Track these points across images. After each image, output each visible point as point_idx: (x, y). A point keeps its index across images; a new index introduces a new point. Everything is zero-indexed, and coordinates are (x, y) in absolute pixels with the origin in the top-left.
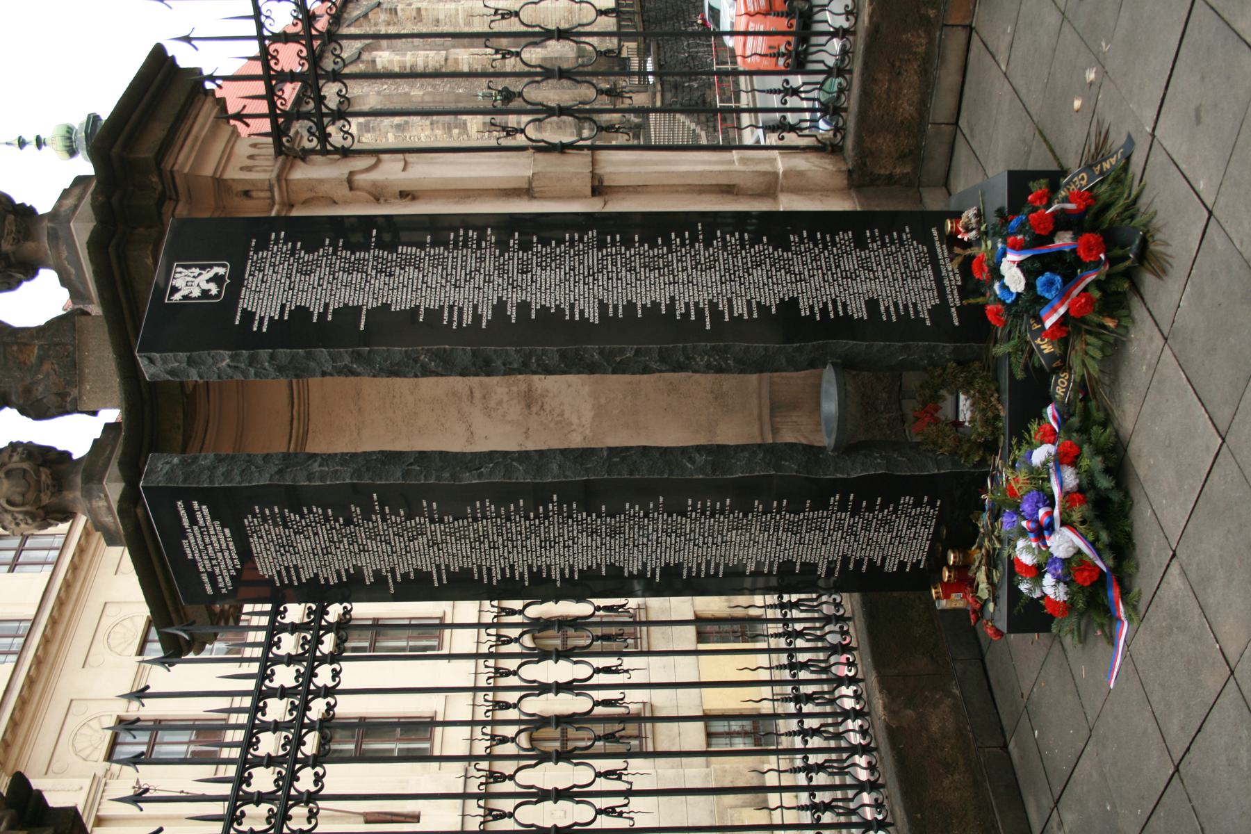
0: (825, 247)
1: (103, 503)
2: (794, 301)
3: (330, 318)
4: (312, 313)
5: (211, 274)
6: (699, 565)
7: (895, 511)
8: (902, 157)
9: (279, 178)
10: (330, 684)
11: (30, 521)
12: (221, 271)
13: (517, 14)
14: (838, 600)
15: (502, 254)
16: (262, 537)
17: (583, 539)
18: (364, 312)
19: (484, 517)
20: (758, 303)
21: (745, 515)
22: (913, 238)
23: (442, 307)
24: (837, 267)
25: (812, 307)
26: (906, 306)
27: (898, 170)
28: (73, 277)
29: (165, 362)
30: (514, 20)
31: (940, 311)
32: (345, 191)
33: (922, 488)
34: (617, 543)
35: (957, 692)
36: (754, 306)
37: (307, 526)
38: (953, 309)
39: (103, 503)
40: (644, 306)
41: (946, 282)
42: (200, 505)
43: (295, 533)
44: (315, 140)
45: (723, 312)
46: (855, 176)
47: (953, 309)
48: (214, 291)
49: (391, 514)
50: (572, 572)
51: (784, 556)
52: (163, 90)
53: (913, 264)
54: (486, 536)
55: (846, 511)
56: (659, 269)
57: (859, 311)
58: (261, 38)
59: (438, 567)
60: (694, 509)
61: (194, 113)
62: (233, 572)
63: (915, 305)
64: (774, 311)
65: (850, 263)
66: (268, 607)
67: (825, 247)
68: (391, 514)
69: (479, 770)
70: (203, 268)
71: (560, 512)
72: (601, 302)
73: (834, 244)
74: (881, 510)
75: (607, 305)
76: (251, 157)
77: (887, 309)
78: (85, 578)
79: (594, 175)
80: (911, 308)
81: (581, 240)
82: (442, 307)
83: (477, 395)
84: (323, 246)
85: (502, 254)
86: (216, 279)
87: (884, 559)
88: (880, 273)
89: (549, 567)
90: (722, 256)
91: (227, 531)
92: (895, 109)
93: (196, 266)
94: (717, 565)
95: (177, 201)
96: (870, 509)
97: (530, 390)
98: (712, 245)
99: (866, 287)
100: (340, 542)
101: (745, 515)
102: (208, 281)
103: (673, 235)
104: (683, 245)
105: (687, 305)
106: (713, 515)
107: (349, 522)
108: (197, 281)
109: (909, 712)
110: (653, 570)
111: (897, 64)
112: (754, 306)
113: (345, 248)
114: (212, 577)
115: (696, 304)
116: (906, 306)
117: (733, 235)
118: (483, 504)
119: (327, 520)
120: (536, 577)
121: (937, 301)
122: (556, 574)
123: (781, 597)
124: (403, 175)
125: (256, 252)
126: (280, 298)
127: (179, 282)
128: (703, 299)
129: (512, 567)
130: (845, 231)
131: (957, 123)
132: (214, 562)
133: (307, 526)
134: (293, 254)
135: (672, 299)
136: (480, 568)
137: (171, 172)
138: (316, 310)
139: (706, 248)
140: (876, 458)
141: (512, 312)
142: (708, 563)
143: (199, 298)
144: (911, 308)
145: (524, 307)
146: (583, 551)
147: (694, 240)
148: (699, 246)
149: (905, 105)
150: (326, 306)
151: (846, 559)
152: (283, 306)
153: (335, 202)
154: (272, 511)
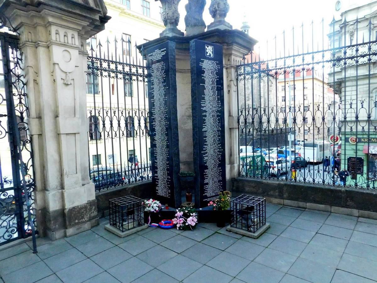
0: (219, 174)
2: (208, 169)
7: (167, 189)
12: (212, 56)
25: (206, 172)
26: (207, 190)
40: (206, 139)
67: (219, 174)
70: (212, 52)
71: (166, 124)
76: (236, 61)
77: (206, 187)
81: (219, 127)
86: (210, 55)
89: (155, 122)
94: (156, 154)
99: (211, 182)
105: (206, 148)
110: (155, 142)
113: (217, 80)
115: (207, 150)
116: (207, 190)
119: (163, 78)
122: (154, 123)
124: (233, 91)
135: (208, 145)
138: (204, 75)
145: (205, 116)
152: (205, 68)
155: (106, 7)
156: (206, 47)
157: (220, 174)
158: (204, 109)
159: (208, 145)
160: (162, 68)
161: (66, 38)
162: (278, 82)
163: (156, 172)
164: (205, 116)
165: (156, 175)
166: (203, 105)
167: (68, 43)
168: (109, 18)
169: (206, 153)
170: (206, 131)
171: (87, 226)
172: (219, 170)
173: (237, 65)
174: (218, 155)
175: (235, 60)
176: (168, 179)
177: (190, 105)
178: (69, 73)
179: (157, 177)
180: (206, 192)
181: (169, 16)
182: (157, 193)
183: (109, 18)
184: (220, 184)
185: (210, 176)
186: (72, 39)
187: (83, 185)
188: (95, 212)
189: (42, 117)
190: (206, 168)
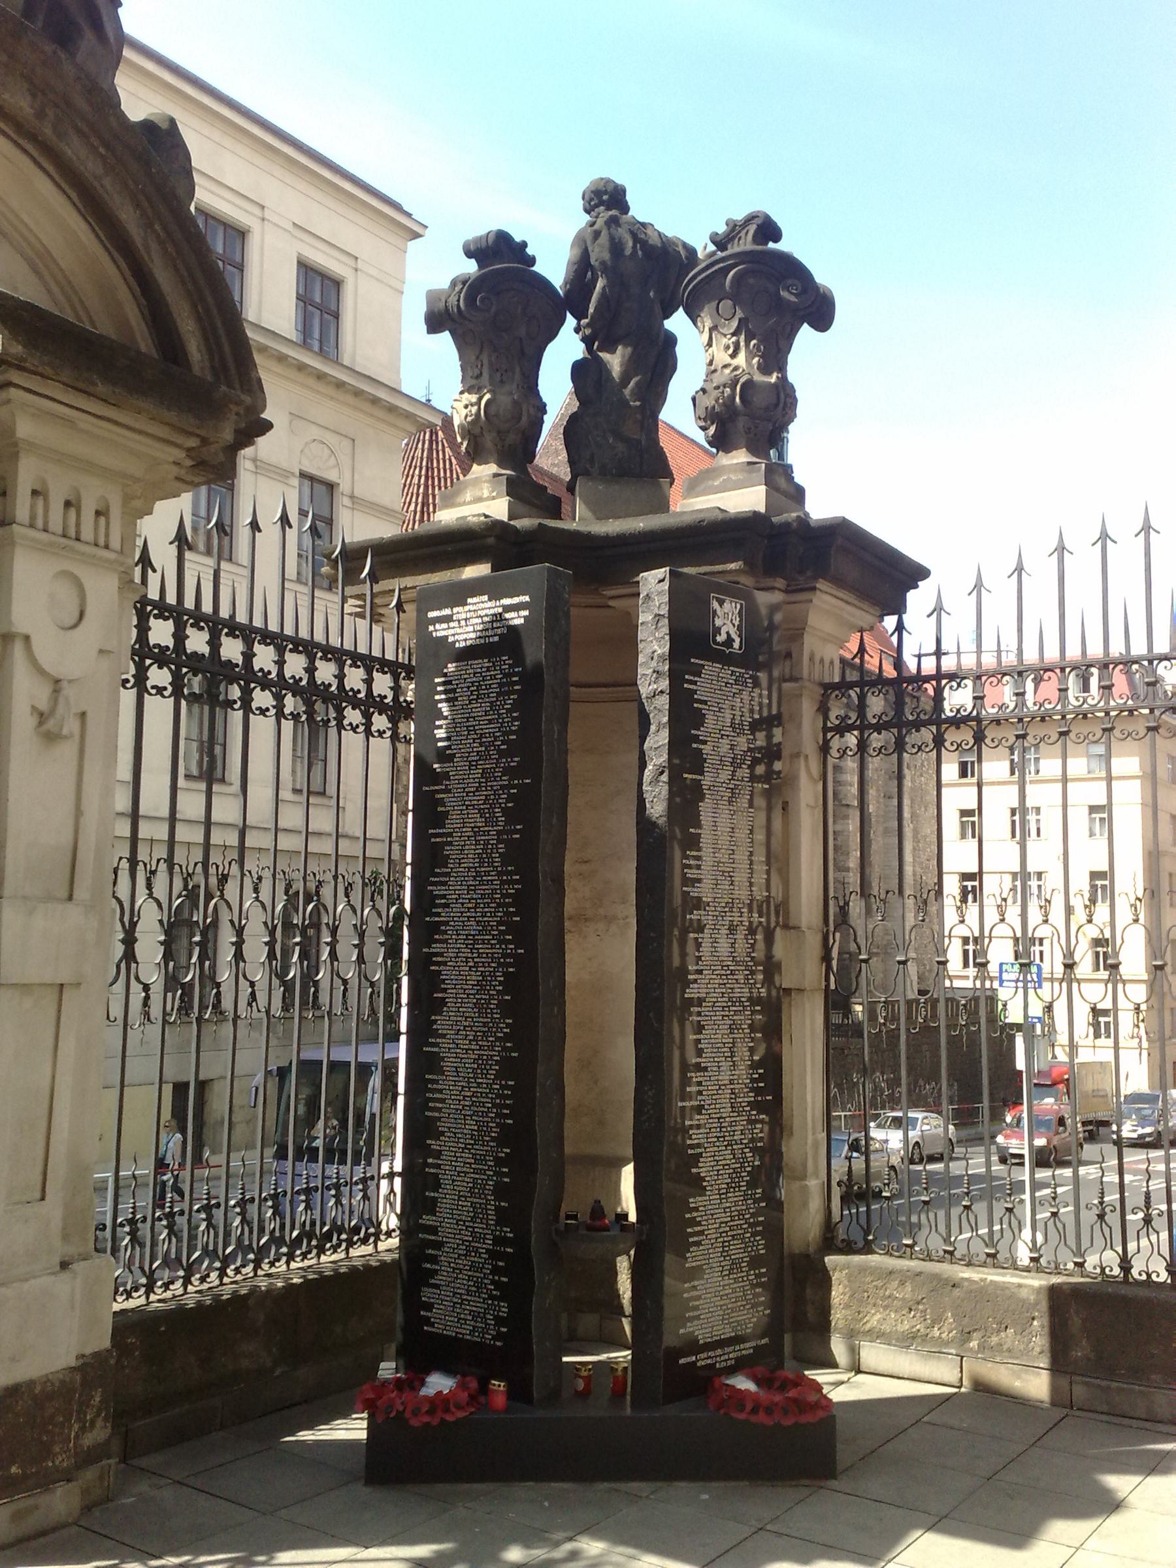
0: (751, 1225)
1: (486, 494)
3: (694, 746)
4: (699, 730)
5: (734, 636)
6: (440, 1091)
7: (491, 1297)
11: (469, 419)
12: (736, 645)
14: (393, 1234)
16: (488, 670)
17: (475, 977)
19: (503, 882)
21: (493, 1139)
24: (733, 1236)
25: (696, 1209)
26: (696, 1308)
28: (710, 483)
29: (659, 593)
33: (518, 1323)
34: (468, 1009)
36: (699, 1150)
37: (499, 714)
38: (694, 1358)
39: (486, 494)
41: (719, 1352)
42: (525, 617)
43: (491, 703)
44: (837, 722)
47: (694, 1358)
48: (719, 639)
49: (509, 794)
50: (438, 964)
51: (445, 1180)
52: (885, 577)
54: (482, 883)
55: (493, 1245)
56: (732, 1057)
58: (939, 676)
59: (450, 835)
60: (503, 1087)
61: (865, 607)
62: (451, 639)
63: (698, 1317)
64: (694, 1170)
68: (509, 794)
69: (230, 864)
70: (739, 628)
71: (505, 956)
73: (754, 1234)
74: (493, 1282)
76: (822, 661)
78: (65, 192)
80: (696, 1313)
82: (699, 850)
83: (584, 867)
86: (729, 641)
87: (437, 1286)
88: (726, 1282)
89: (445, 941)
91: (496, 639)
93: (741, 621)
94: (439, 1110)
95: (786, 591)
96: (495, 1270)
97: (586, 920)
98: (752, 1110)
100: (481, 745)
101: (493, 1139)
102: (728, 633)
103: (761, 1071)
106: (494, 1105)
107: (502, 754)
108: (729, 622)
109: (262, 1317)
110: (436, 1045)
111: (921, 1307)
112: (699, 1150)
114: (448, 619)
118: (516, 882)
119: (505, 734)
120: (435, 928)
121: (701, 1342)
122: (436, 948)
123: (399, 1174)
124: (803, 805)
127: (727, 605)
129: (446, 906)
130: (766, 1247)
132: (463, 623)
133: (499, 714)
135: (705, 1069)
136: (448, 875)
137: (814, 589)
138: (700, 733)
142: (443, 1101)
143: (714, 625)
144: (696, 1313)
146: (460, 976)
149: (878, 1316)
151: (439, 1245)
152: (705, 702)
154: (516, 683)
155: (259, 380)
156: (715, 605)
157: (758, 1224)
159: (705, 1069)
160: (500, 685)
161: (40, 503)
162: (1031, 782)
163: (431, 1207)
165: (427, 1220)
167: (78, 539)
168: (267, 426)
170: (700, 1002)
171: (61, 1501)
173: (827, 681)
175: (817, 659)
176: (497, 1241)
178: (70, 681)
179: (433, 1230)
181: (497, 415)
182: (427, 1320)
183: (267, 426)
184: (757, 1276)
185: (712, 1233)
186: (96, 522)
187: (64, 1265)
188: (99, 1423)
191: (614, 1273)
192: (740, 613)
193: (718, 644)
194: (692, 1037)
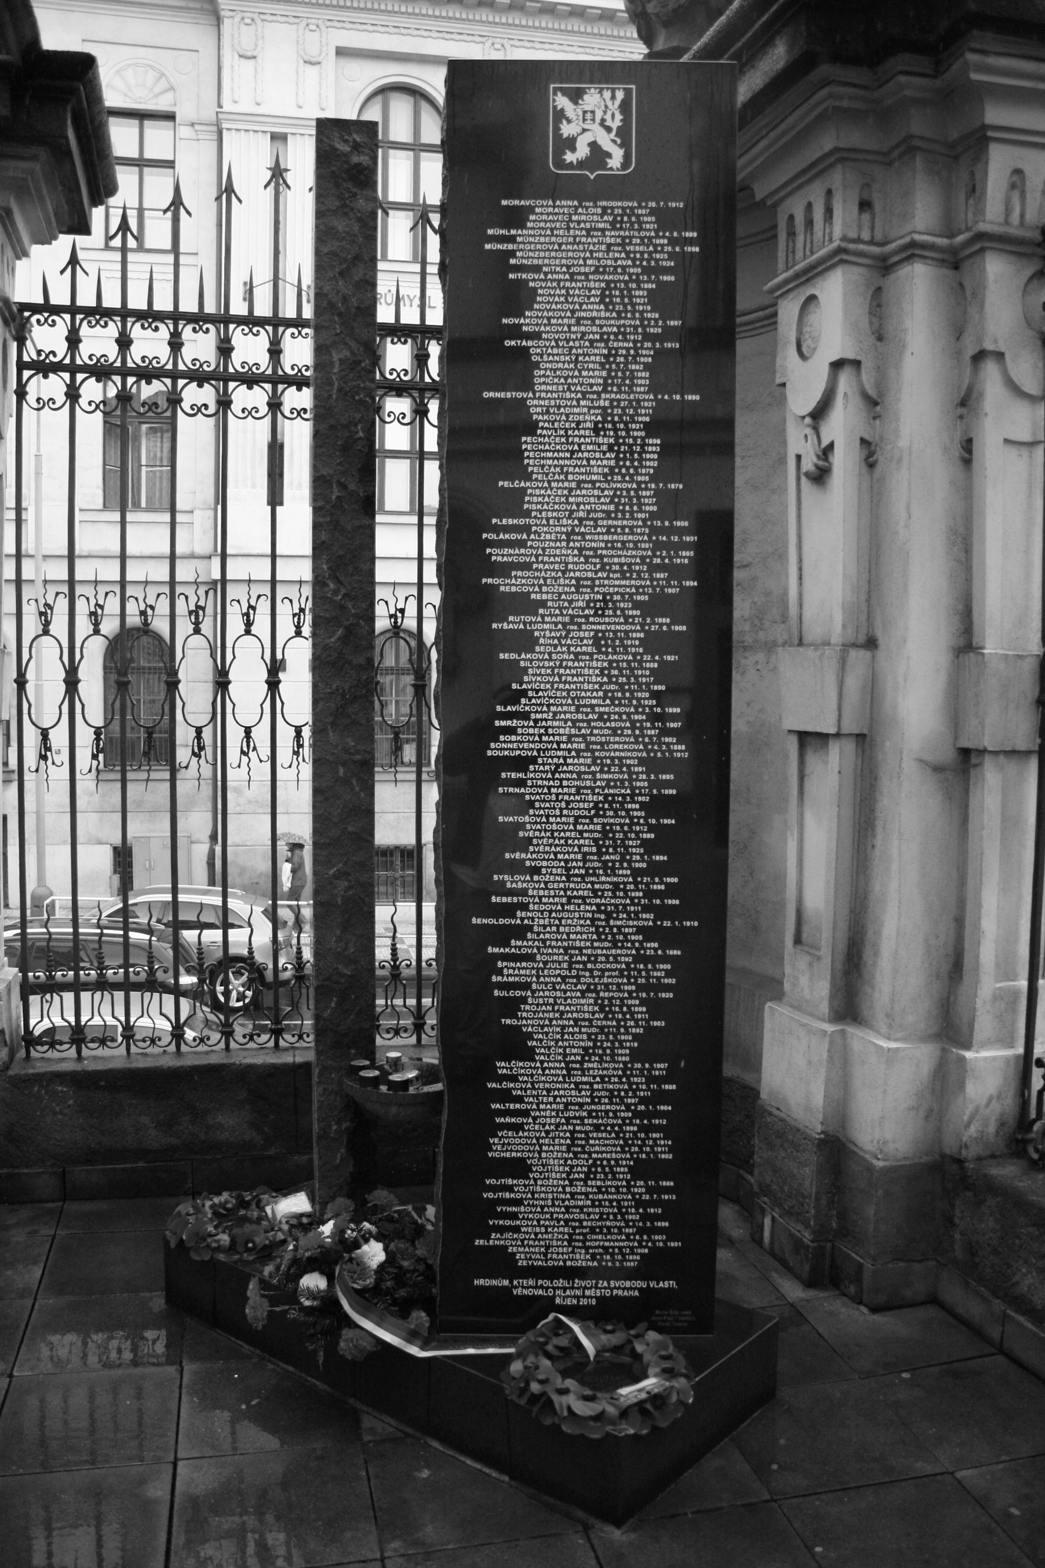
2: (529, 1055)
8: (971, 1249)
9: (981, 236)
10: (286, 409)
12: (616, 160)
13: (46, 632)
15: (637, 605)
18: (520, 395)
20: (524, 1000)
22: (654, 1250)
23: (527, 514)
25: (514, 1078)
26: (514, 1216)
27: (957, 1236)
30: (191, 628)
31: (503, 1263)
32: (971, 351)
35: (271, 1152)
36: (518, 993)
38: (506, 1283)
40: (522, 826)
41: (561, 1283)
45: (509, 946)
46: (955, 1168)
47: (506, 1283)
53: (597, 1241)
57: (503, 1146)
63: (517, 1229)
65: (604, 1147)
66: (308, 313)
67: (636, 1114)
70: (623, 133)
72: (533, 760)
75: (526, 770)
77: (510, 1189)
79: (982, 752)
81: (665, 732)
82: (527, 514)
84: (664, 317)
85: (637, 605)
90: (626, 956)
92: (1026, 1262)
99: (553, 1164)
104: (649, 894)
105: (524, 892)
112: (518, 993)
113: (658, 354)
115: (525, 907)
116: (514, 1216)
117: (668, 974)
125: (653, 212)
126: (554, 263)
128: (534, 917)
131: (1001, 1351)
134: (647, 271)
138: (528, 322)
139: (640, 930)
140: (338, 1123)
141: (513, 623)
143: (555, 107)
145: (526, 641)
147: (661, 912)
148: (648, 919)
150: (536, 336)
152: (537, 269)
153: (958, 339)
158: (508, 586)
159: (536, 870)
164: (526, 641)
166: (498, 555)
169: (521, 932)
170: (522, 763)
172: (650, 1079)
174: (638, 958)
177: (675, 572)
180: (502, 1230)
185: (548, 1114)
189: (881, 642)
190: (518, 1047)
191: (428, 1093)
192: (625, 107)
193: (570, 166)
194: (413, 719)
